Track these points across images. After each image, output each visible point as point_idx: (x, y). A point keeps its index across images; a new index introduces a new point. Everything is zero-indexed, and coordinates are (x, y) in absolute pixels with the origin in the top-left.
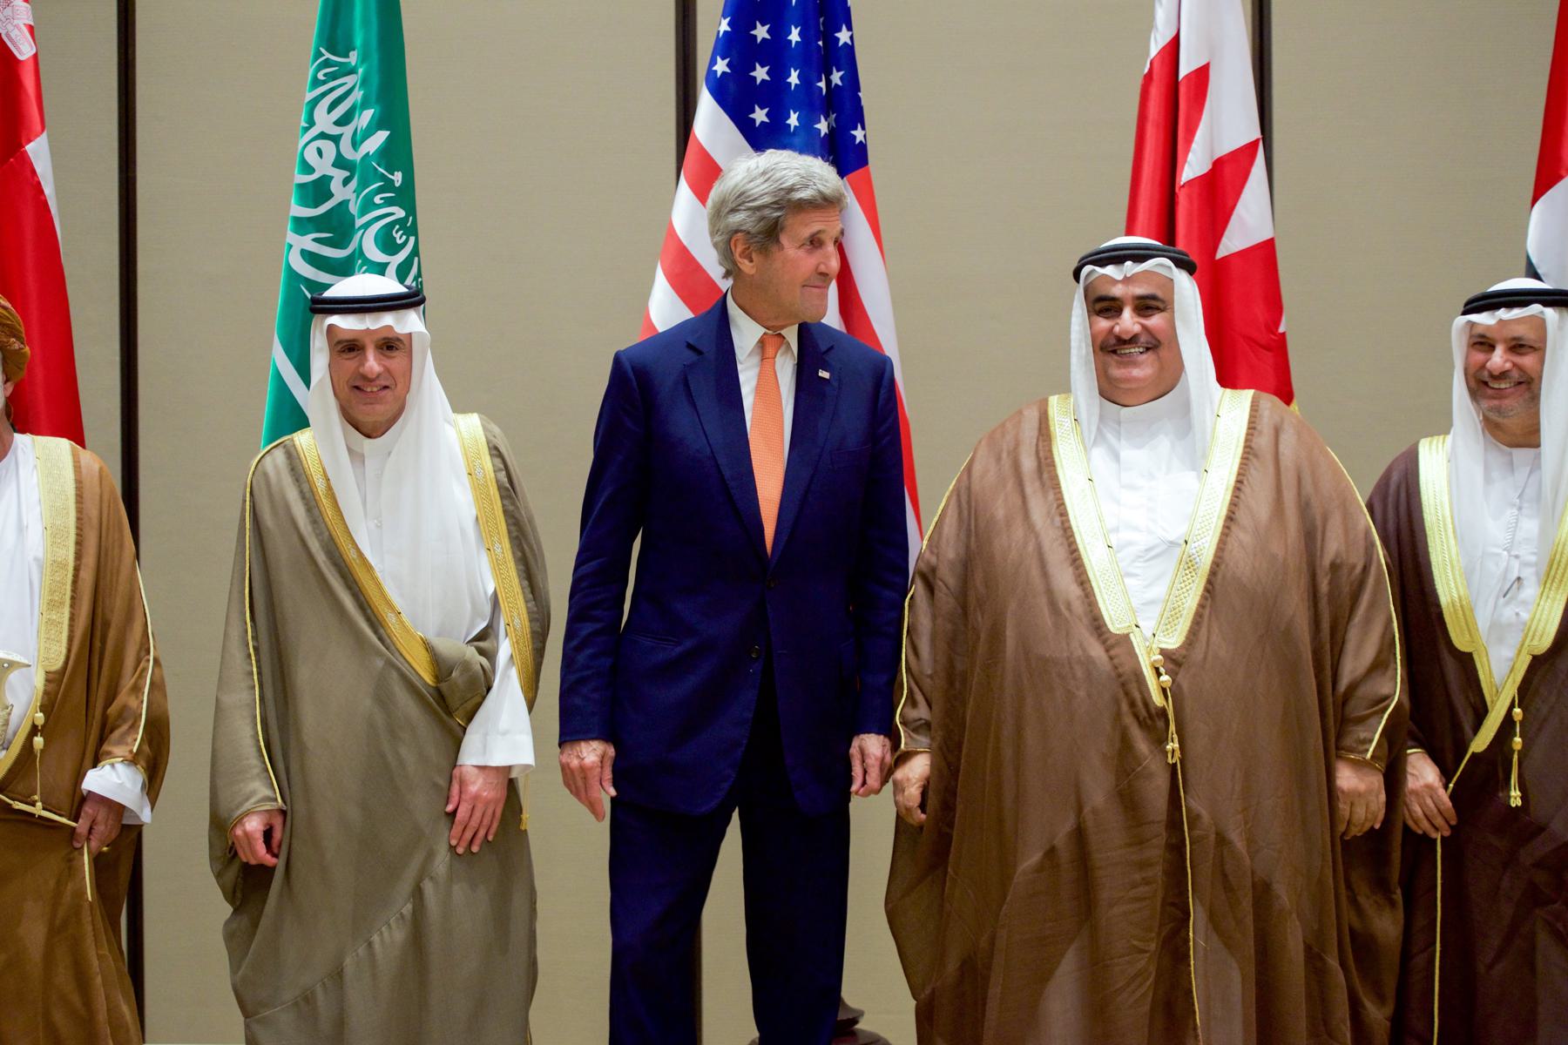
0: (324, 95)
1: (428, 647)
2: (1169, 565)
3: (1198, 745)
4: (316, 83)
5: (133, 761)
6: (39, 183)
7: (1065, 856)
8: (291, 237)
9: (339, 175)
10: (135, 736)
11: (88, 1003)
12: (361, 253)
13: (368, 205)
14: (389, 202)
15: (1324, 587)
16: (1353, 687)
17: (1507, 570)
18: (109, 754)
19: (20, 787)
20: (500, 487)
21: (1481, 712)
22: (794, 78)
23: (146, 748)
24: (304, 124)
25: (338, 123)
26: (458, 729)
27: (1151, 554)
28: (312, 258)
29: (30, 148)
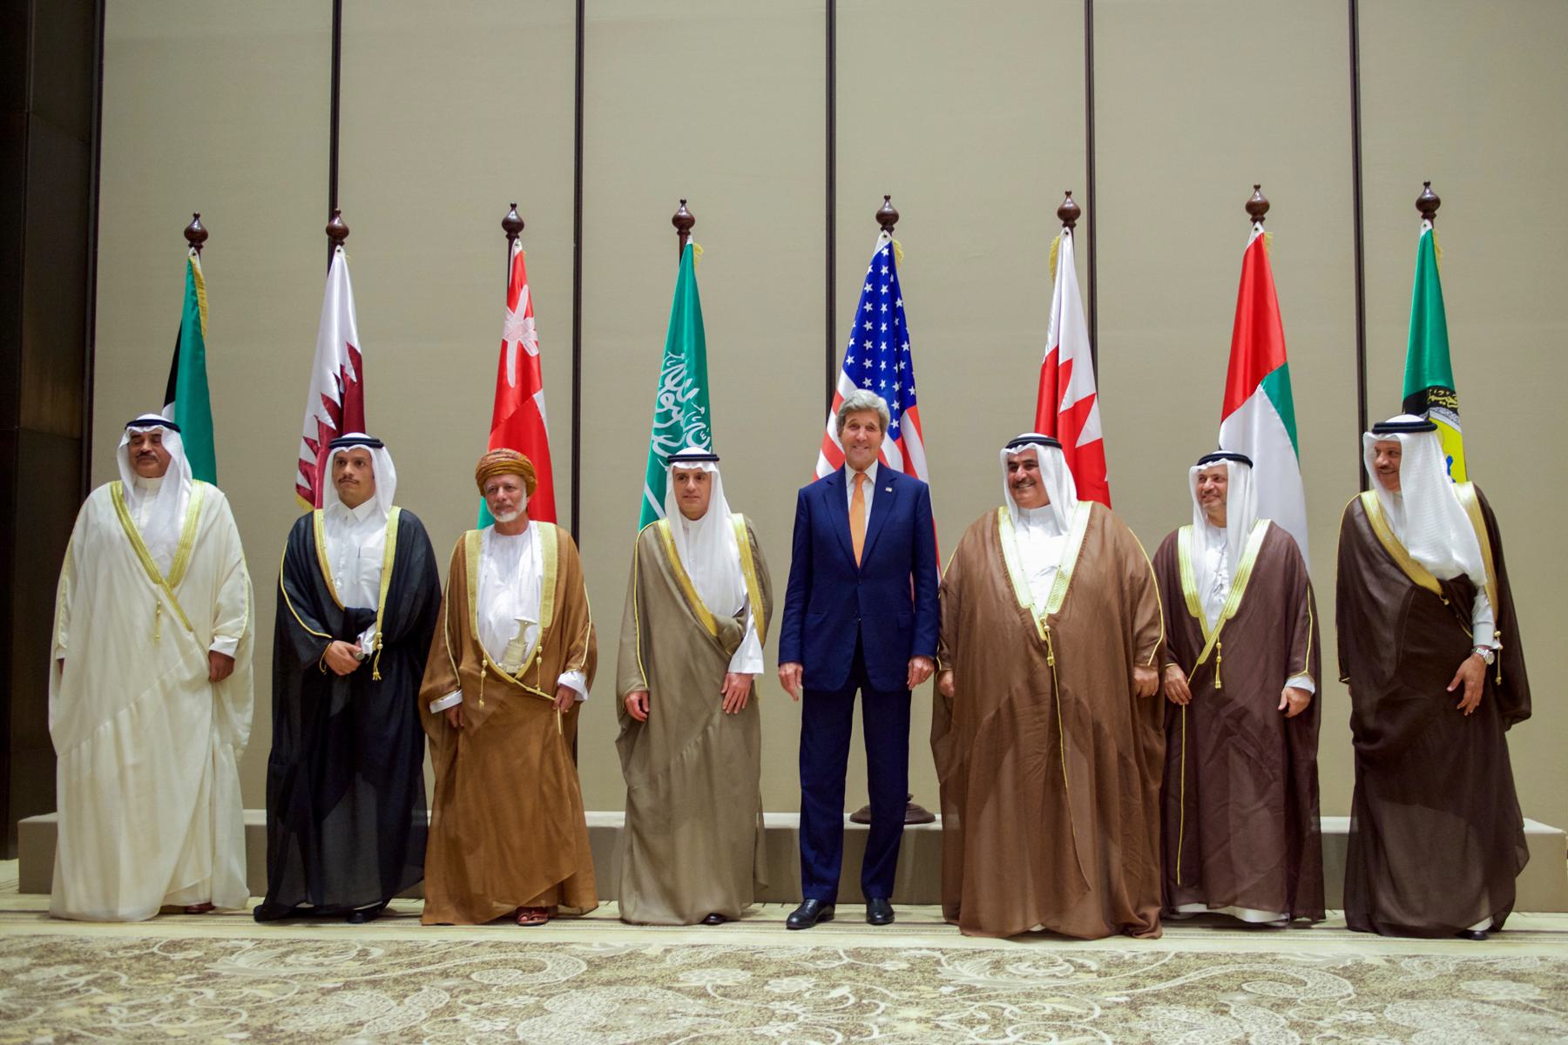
0: (669, 373)
2: (1052, 577)
3: (1066, 658)
4: (666, 367)
5: (581, 670)
7: (1004, 711)
8: (654, 437)
9: (676, 409)
11: (559, 780)
13: (689, 422)
14: (698, 421)
15: (1127, 587)
16: (1141, 632)
17: (1216, 581)
18: (570, 667)
19: (530, 681)
20: (751, 546)
21: (1202, 644)
22: (883, 365)
23: (587, 666)
24: (660, 386)
25: (675, 386)
27: (1044, 573)
29: (535, 396)
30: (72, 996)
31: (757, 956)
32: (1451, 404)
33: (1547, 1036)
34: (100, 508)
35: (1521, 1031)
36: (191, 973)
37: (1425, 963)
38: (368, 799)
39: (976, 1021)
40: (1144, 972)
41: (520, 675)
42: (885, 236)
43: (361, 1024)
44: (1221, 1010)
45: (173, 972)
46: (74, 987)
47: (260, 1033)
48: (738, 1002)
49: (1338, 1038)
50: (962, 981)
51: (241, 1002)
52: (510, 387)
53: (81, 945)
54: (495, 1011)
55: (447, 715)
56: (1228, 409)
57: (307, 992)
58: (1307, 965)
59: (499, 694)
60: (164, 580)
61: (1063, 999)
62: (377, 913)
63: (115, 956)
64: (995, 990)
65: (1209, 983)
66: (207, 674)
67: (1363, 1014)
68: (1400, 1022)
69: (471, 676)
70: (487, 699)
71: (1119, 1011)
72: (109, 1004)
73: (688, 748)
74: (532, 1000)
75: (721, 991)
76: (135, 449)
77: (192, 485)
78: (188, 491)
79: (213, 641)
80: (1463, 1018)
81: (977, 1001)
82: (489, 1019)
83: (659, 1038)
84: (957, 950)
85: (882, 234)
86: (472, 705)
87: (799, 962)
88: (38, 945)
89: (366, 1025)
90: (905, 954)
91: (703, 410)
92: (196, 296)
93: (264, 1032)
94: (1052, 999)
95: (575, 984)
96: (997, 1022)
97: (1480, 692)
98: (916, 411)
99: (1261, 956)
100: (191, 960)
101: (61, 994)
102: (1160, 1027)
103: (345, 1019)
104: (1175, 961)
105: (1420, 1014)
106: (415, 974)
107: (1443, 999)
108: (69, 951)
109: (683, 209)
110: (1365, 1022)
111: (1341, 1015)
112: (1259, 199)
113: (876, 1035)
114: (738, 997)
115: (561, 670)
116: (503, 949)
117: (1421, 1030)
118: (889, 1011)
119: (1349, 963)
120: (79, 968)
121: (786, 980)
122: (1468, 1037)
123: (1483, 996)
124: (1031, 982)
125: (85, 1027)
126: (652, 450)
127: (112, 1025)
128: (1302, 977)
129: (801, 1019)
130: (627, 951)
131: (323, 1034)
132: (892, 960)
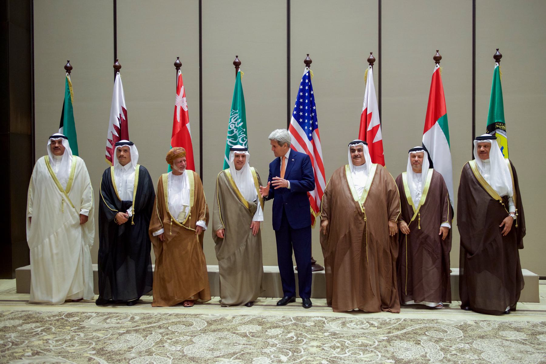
0: (233, 117)
1: (248, 203)
4: (232, 115)
5: (204, 220)
6: (188, 131)
8: (228, 139)
9: (235, 129)
10: (156, 217)
12: (239, 142)
13: (240, 134)
14: (243, 134)
17: (417, 193)
20: (258, 178)
21: (413, 214)
22: (306, 114)
23: (206, 218)
24: (230, 121)
25: (235, 121)
26: (252, 216)
28: (231, 142)
29: (187, 125)
30: (37, 336)
31: (264, 319)
32: (503, 128)
33: (527, 354)
34: (41, 166)
35: (518, 352)
36: (76, 327)
37: (488, 324)
38: (132, 264)
39: (336, 347)
40: (393, 327)
41: (184, 223)
42: (307, 69)
43: (132, 348)
44: (418, 343)
45: (69, 326)
46: (37, 332)
47: (99, 351)
48: (257, 339)
49: (457, 355)
50: (332, 330)
51: (93, 338)
52: (178, 122)
53: (38, 315)
54: (176, 342)
55: (159, 237)
56: (426, 130)
57: (114, 334)
58: (448, 324)
59: (177, 229)
60: (64, 191)
61: (365, 338)
62: (137, 302)
63: (50, 319)
64: (343, 334)
65: (415, 331)
66: (79, 222)
67: (465, 345)
68: (478, 348)
69: (167, 224)
70: (173, 232)
71: (384, 343)
72: (49, 339)
73: (242, 247)
74: (189, 338)
75: (251, 334)
76: (53, 146)
77: (72, 158)
78: (71, 160)
79: (81, 211)
80: (499, 347)
81: (336, 339)
82: (175, 346)
83: (231, 354)
84: (330, 317)
85: (306, 68)
86: (168, 234)
87: (277, 322)
88: (24, 315)
89: (134, 348)
90: (313, 319)
91: (244, 130)
92: (69, 90)
93: (100, 351)
94: (361, 338)
95: (203, 331)
96: (343, 347)
97: (510, 229)
98: (318, 130)
99: (433, 320)
100: (75, 321)
101: (33, 335)
102: (397, 349)
103: (127, 346)
104: (404, 322)
105: (485, 345)
106: (150, 327)
107: (493, 339)
108: (34, 317)
109: (237, 59)
110: (466, 348)
111: (458, 345)
112: (438, 55)
113: (302, 353)
114: (257, 337)
115: (197, 220)
116: (179, 317)
117: (484, 352)
118: (307, 342)
119: (462, 323)
120: (38, 324)
121: (273, 330)
122: (500, 355)
123: (506, 337)
124: (354, 331)
125: (42, 349)
126: (227, 144)
127: (50, 348)
128: (446, 329)
129: (278, 346)
130: (220, 318)
131: (120, 352)
132: (309, 321)
